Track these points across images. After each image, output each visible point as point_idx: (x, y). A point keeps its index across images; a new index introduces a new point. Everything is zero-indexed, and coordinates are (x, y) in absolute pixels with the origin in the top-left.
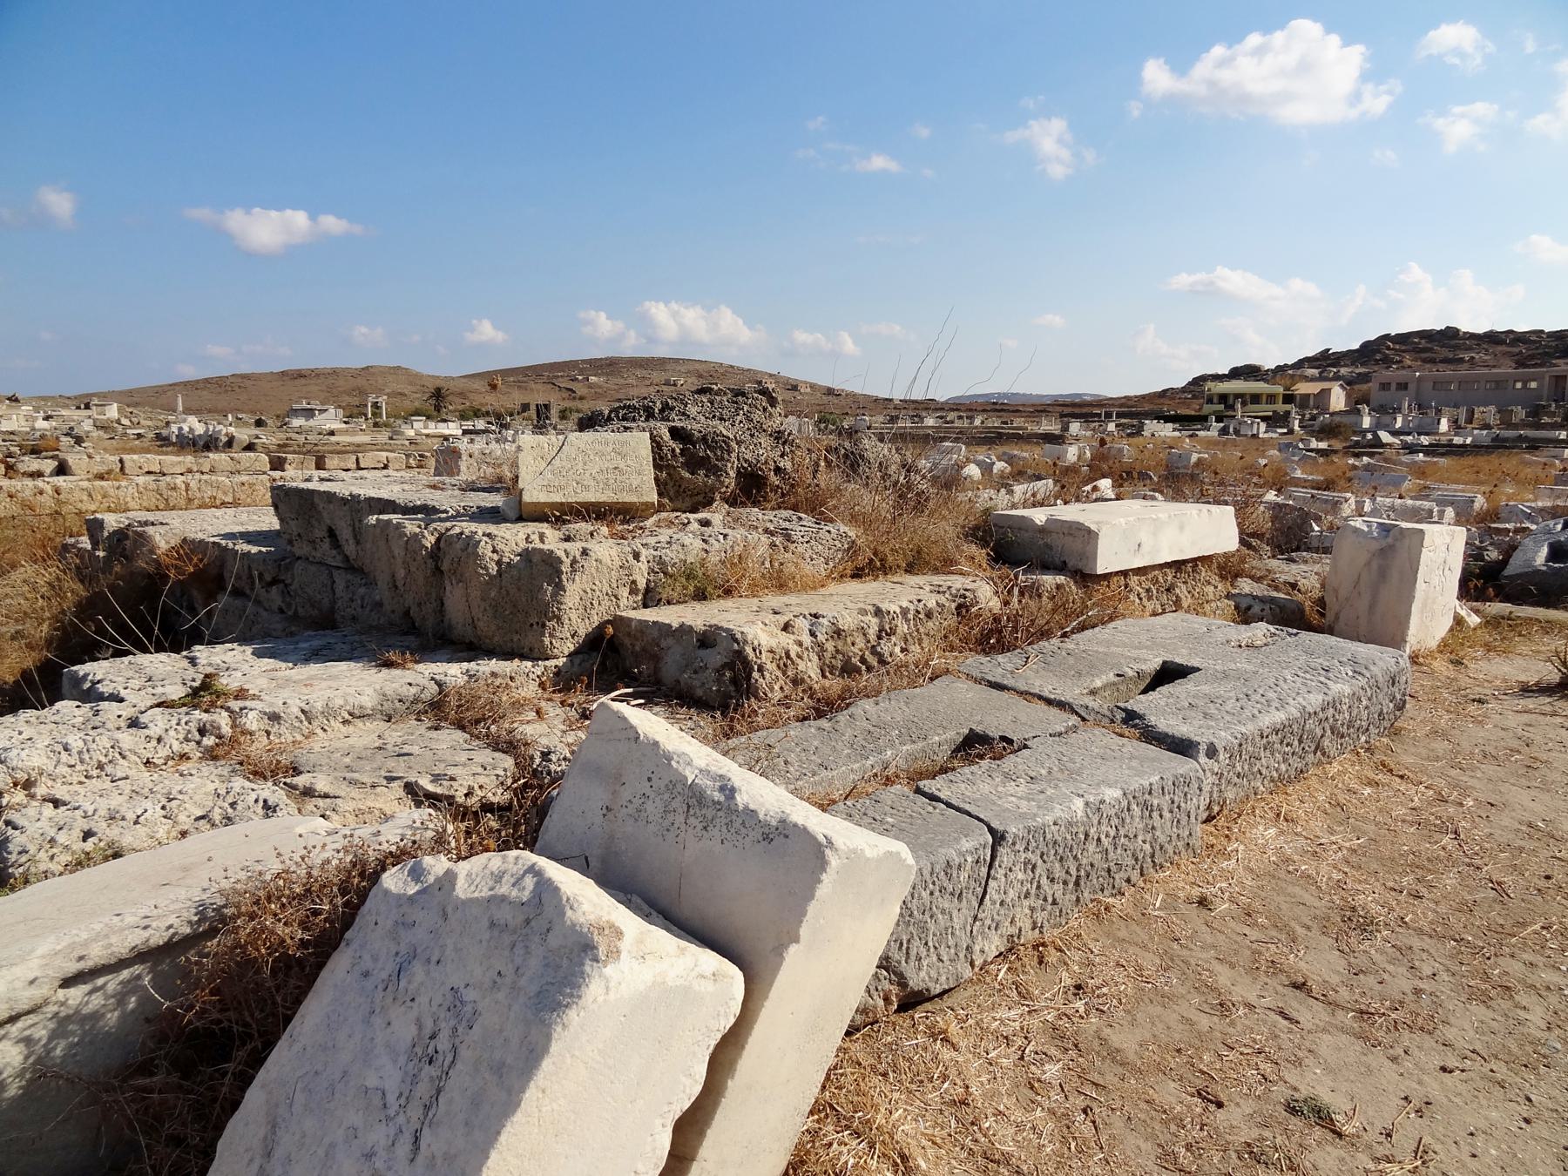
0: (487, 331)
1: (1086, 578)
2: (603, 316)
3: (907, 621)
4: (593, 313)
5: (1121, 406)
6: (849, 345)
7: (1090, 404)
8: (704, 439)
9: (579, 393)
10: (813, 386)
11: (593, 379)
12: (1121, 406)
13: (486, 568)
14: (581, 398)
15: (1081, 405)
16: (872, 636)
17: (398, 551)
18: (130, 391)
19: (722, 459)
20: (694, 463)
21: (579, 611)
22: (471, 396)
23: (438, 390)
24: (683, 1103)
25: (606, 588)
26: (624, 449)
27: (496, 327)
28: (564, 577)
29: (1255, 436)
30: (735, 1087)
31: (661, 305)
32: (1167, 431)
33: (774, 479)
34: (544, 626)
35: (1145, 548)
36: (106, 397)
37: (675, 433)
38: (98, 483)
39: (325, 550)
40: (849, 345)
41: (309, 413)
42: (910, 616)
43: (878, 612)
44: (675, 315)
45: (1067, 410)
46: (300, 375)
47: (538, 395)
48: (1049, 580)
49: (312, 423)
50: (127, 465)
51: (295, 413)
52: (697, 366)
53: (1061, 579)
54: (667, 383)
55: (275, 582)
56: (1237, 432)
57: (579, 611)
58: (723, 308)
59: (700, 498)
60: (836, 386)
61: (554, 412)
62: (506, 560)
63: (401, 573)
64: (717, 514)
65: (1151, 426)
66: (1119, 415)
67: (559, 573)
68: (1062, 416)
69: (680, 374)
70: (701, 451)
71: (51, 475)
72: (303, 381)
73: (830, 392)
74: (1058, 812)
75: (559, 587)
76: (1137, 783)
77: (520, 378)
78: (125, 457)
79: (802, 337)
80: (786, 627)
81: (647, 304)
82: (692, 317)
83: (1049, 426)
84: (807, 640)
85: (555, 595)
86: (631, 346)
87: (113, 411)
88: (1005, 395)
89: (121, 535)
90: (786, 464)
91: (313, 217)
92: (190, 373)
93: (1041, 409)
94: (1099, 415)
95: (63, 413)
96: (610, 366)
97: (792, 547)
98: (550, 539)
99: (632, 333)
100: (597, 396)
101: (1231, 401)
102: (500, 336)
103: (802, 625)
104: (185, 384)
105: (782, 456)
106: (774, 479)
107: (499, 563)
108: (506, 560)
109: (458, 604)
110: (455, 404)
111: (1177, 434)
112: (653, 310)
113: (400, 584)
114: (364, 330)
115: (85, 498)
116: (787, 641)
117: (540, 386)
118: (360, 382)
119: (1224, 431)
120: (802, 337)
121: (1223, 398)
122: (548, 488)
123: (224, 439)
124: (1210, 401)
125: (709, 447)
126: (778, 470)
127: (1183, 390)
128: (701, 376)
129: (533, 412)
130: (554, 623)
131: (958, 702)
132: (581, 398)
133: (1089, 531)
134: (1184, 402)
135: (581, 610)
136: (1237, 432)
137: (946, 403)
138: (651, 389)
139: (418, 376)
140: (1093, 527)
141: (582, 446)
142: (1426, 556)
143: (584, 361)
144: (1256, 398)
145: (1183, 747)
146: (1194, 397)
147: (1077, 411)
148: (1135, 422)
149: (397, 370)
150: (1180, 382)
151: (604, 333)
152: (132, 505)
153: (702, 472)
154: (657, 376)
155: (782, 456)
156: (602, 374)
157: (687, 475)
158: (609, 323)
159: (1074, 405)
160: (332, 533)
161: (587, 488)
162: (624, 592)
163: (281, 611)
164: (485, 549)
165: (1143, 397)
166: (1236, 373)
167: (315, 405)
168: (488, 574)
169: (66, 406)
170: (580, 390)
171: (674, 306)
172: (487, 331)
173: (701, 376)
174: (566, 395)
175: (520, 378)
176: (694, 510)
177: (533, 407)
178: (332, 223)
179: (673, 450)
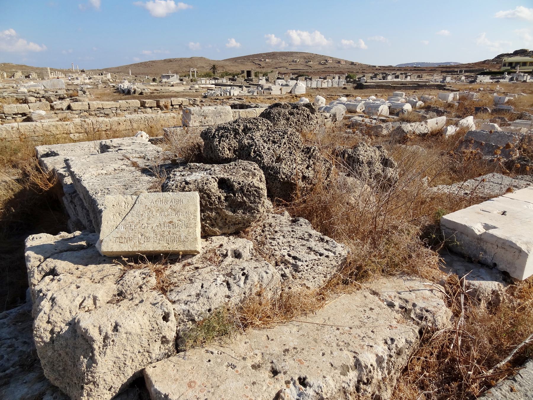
0: (233, 43)
2: (273, 36)
3: (382, 368)
4: (270, 35)
5: (466, 67)
6: (363, 45)
7: (454, 67)
8: (241, 190)
9: (262, 66)
10: (346, 61)
11: (267, 60)
12: (466, 67)
13: (41, 337)
14: (263, 67)
15: (449, 67)
18: (118, 67)
19: (255, 202)
20: (234, 206)
22: (225, 67)
23: (214, 66)
25: (137, 348)
26: (178, 207)
27: (236, 41)
28: (96, 353)
29: (525, 81)
31: (294, 31)
32: (487, 79)
33: (301, 184)
34: (82, 388)
36: (107, 70)
37: (223, 184)
38: (60, 123)
40: (363, 45)
41: (168, 77)
42: (384, 365)
44: (299, 35)
45: (444, 70)
46: (170, 61)
47: (249, 67)
48: (489, 286)
49: (169, 80)
51: (164, 77)
52: (304, 55)
54: (293, 61)
56: (517, 79)
58: (317, 32)
59: (241, 226)
60: (354, 61)
61: (253, 74)
62: (57, 329)
65: (480, 78)
66: (466, 72)
67: (92, 350)
68: (442, 72)
69: (298, 58)
71: (66, 110)
72: (171, 63)
73: (352, 63)
75: (92, 360)
77: (242, 60)
79: (345, 42)
81: (289, 31)
82: (305, 34)
83: (437, 78)
85: (89, 366)
86: (283, 48)
87: (109, 76)
88: (419, 63)
90: (310, 174)
91: (176, 3)
92: (137, 60)
93: (432, 69)
94: (457, 72)
95: (95, 76)
96: (272, 55)
97: (299, 275)
99: (284, 43)
100: (269, 67)
101: (514, 65)
102: (238, 45)
104: (135, 64)
105: (307, 168)
106: (301, 184)
107: (52, 332)
108: (57, 329)
110: (220, 71)
111: (491, 81)
112: (291, 33)
114: (192, 44)
115: (54, 129)
117: (249, 64)
118: (189, 63)
119: (512, 79)
120: (345, 42)
121: (510, 64)
122: (120, 239)
123: (133, 91)
124: (505, 65)
125: (245, 195)
126: (304, 178)
128: (305, 58)
129: (245, 74)
130: (91, 386)
132: (263, 67)
133: (520, 251)
134: (493, 66)
135: (116, 370)
136: (517, 79)
138: (288, 64)
139: (208, 60)
140: (524, 248)
141: (149, 204)
144: (524, 64)
146: (497, 63)
147: (448, 70)
148: (472, 74)
150: (492, 57)
151: (274, 43)
152: (72, 131)
153: (240, 211)
154: (290, 59)
155: (307, 168)
157: (230, 214)
158: (276, 39)
159: (447, 67)
161: (148, 239)
165: (476, 64)
166: (516, 53)
167: (170, 74)
168: (44, 342)
169: (96, 74)
170: (263, 65)
171: (299, 32)
172: (233, 43)
173: (305, 58)
174: (258, 66)
175: (242, 60)
177: (246, 72)
178: (182, 5)
179: (219, 198)
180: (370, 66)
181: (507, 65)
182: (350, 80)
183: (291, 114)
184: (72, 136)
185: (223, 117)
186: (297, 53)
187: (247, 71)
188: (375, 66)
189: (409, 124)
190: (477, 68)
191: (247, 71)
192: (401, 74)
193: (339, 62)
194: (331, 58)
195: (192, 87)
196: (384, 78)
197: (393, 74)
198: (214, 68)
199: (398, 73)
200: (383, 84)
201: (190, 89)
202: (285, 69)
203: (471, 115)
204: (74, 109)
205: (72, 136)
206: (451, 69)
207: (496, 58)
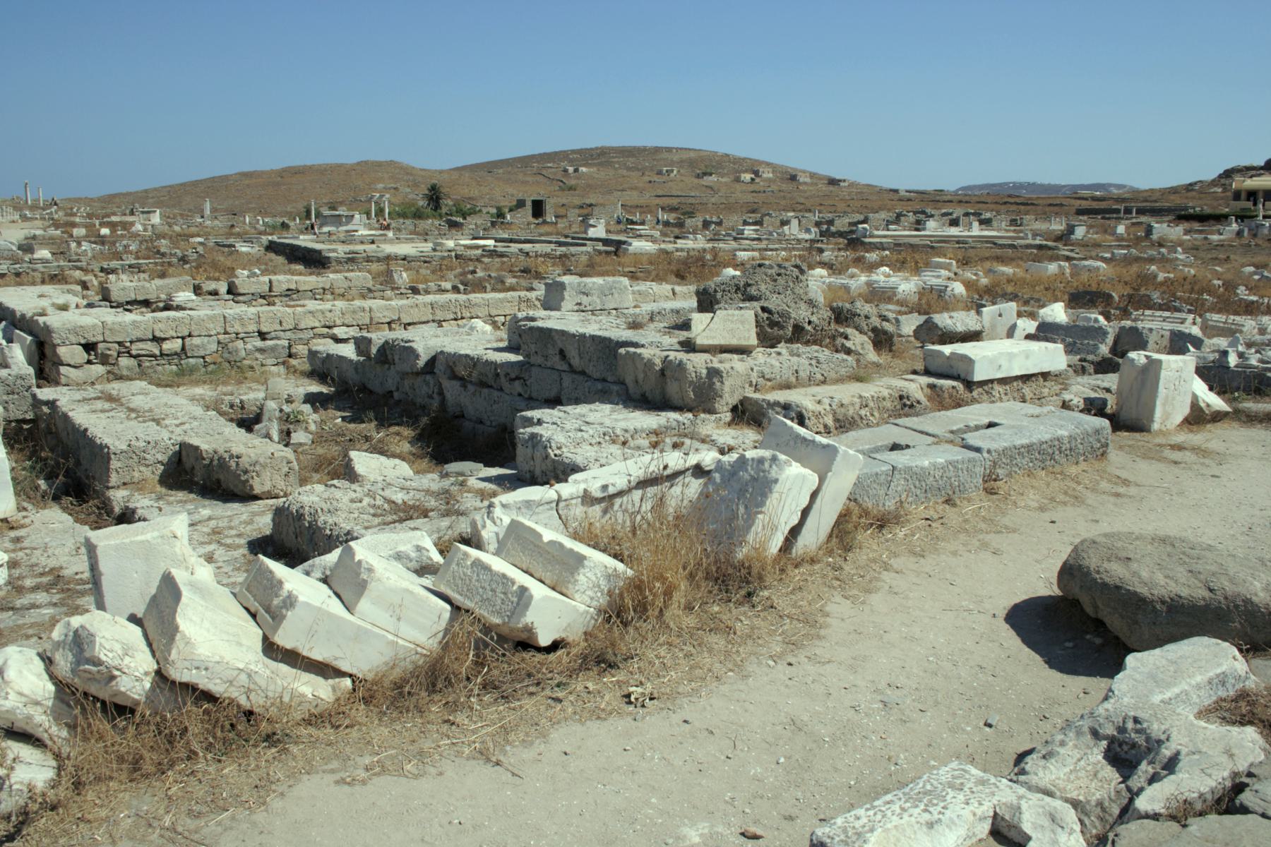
1: (969, 385)
10: (812, 175)
11: (584, 169)
16: (857, 407)
17: (640, 367)
20: (773, 324)
21: (730, 394)
23: (433, 188)
24: (804, 506)
30: (816, 506)
35: (1003, 368)
39: (555, 361)
43: (861, 397)
50: (274, 284)
53: (955, 383)
55: (517, 378)
57: (730, 394)
63: (641, 376)
64: (782, 348)
70: (776, 318)
73: (833, 182)
74: (919, 463)
76: (951, 458)
78: (273, 278)
80: (819, 402)
84: (828, 408)
89: (386, 348)
90: (814, 319)
94: (1118, 211)
98: (715, 362)
103: (827, 401)
109: (673, 389)
113: (640, 381)
116: (819, 408)
126: (810, 322)
127: (1213, 183)
131: (891, 433)
137: (955, 193)
139: (407, 171)
142: (1163, 374)
143: (573, 152)
145: (978, 450)
147: (1095, 205)
149: (391, 163)
152: (338, 322)
156: (594, 165)
160: (562, 352)
162: (747, 386)
163: (520, 395)
164: (689, 366)
176: (772, 347)
180: (881, 191)
181: (1243, 196)
182: (828, 229)
183: (779, 275)
184: (336, 331)
185: (616, 295)
186: (669, 150)
187: (534, 202)
188: (896, 191)
189: (946, 315)
190: (1177, 200)
191: (534, 202)
192: (967, 214)
193: (793, 178)
194: (768, 164)
195: (436, 244)
196: (918, 225)
197: (944, 215)
198: (435, 196)
199: (958, 212)
200: (913, 241)
201: (434, 250)
202: (635, 193)
203: (1056, 300)
204: (242, 291)
205: (336, 331)
206: (1103, 205)
207: (1220, 176)
